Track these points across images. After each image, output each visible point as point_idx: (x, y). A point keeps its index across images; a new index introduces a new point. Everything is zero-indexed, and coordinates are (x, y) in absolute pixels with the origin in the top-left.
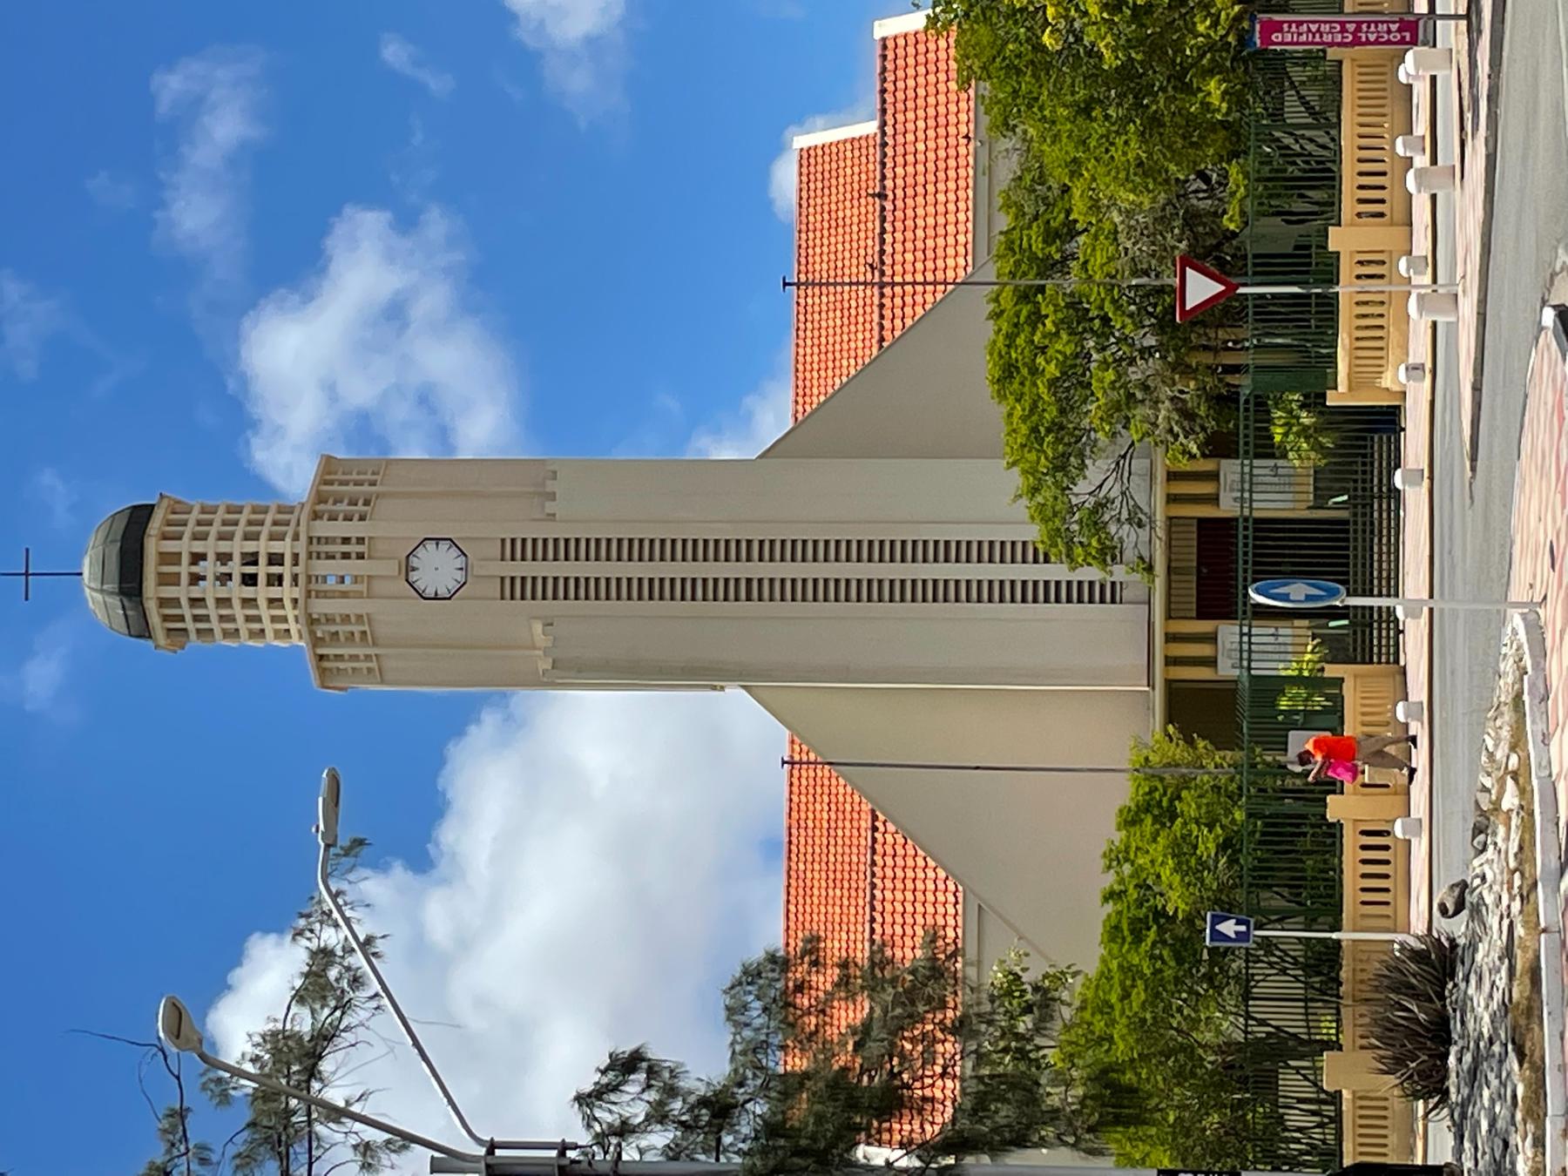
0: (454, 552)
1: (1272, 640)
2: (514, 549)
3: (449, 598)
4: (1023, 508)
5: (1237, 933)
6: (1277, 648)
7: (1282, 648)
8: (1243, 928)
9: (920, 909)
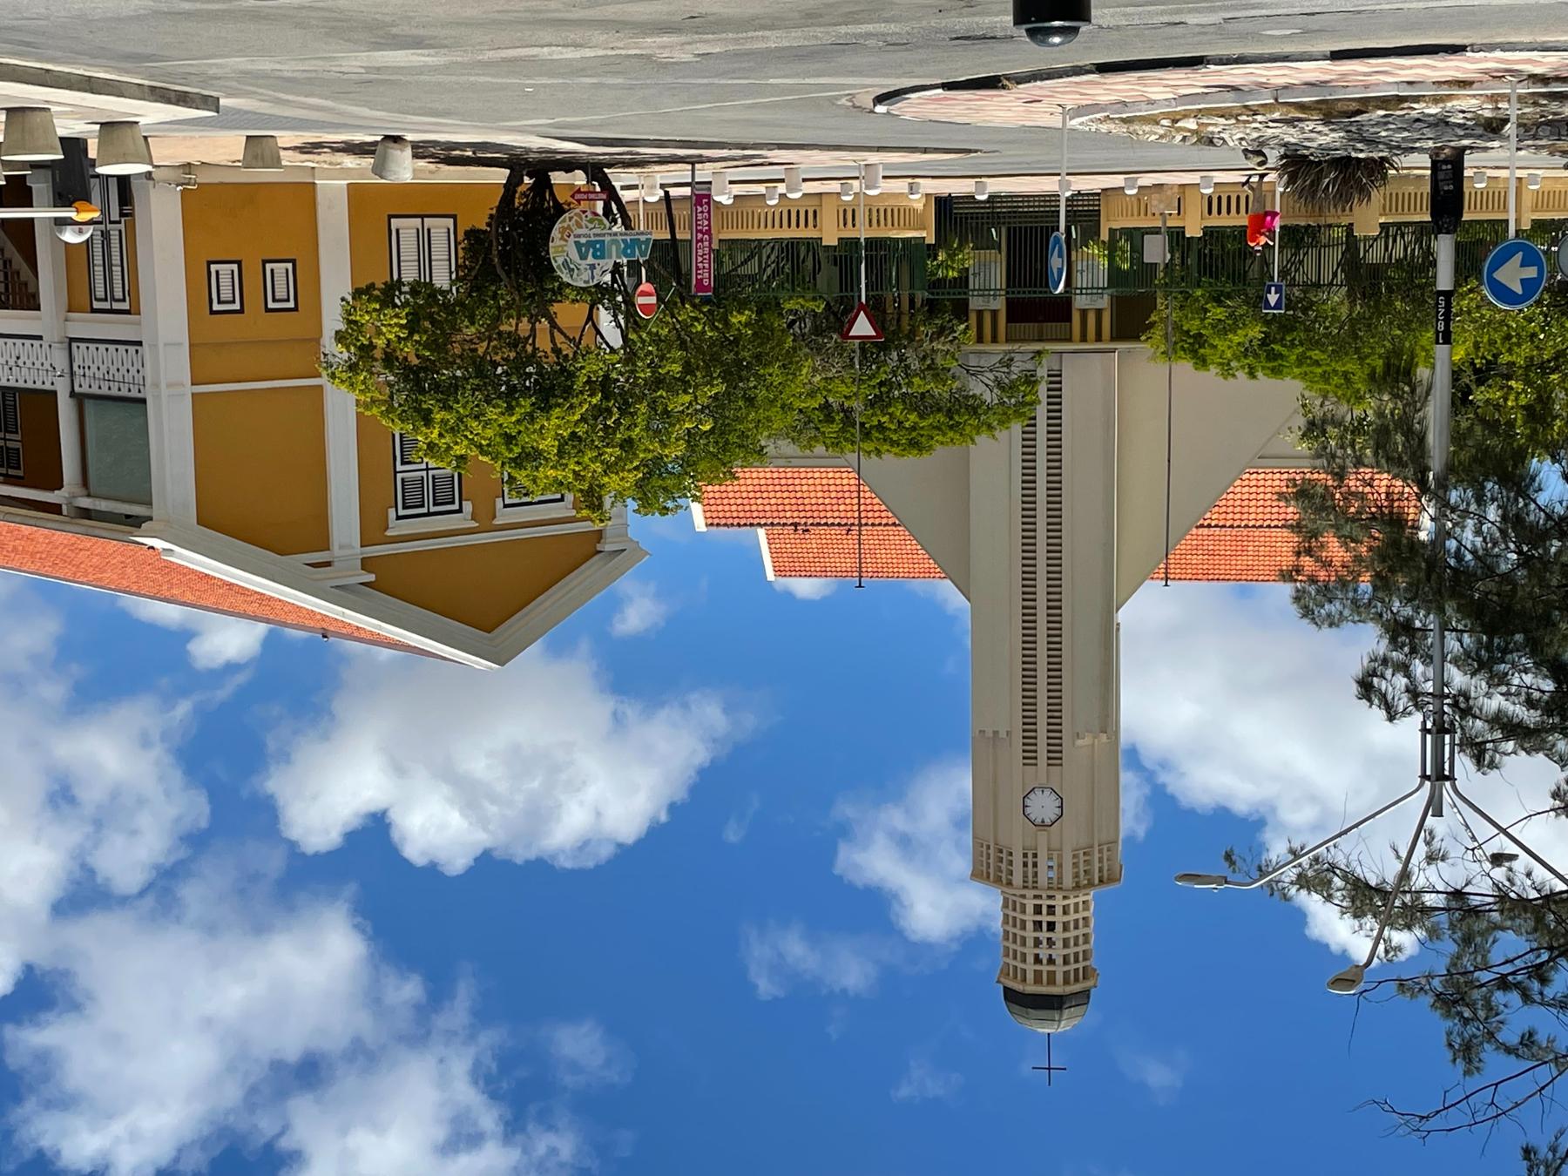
0: (1032, 796)
1: (1085, 274)
4: (1001, 434)
9: (1261, 496)
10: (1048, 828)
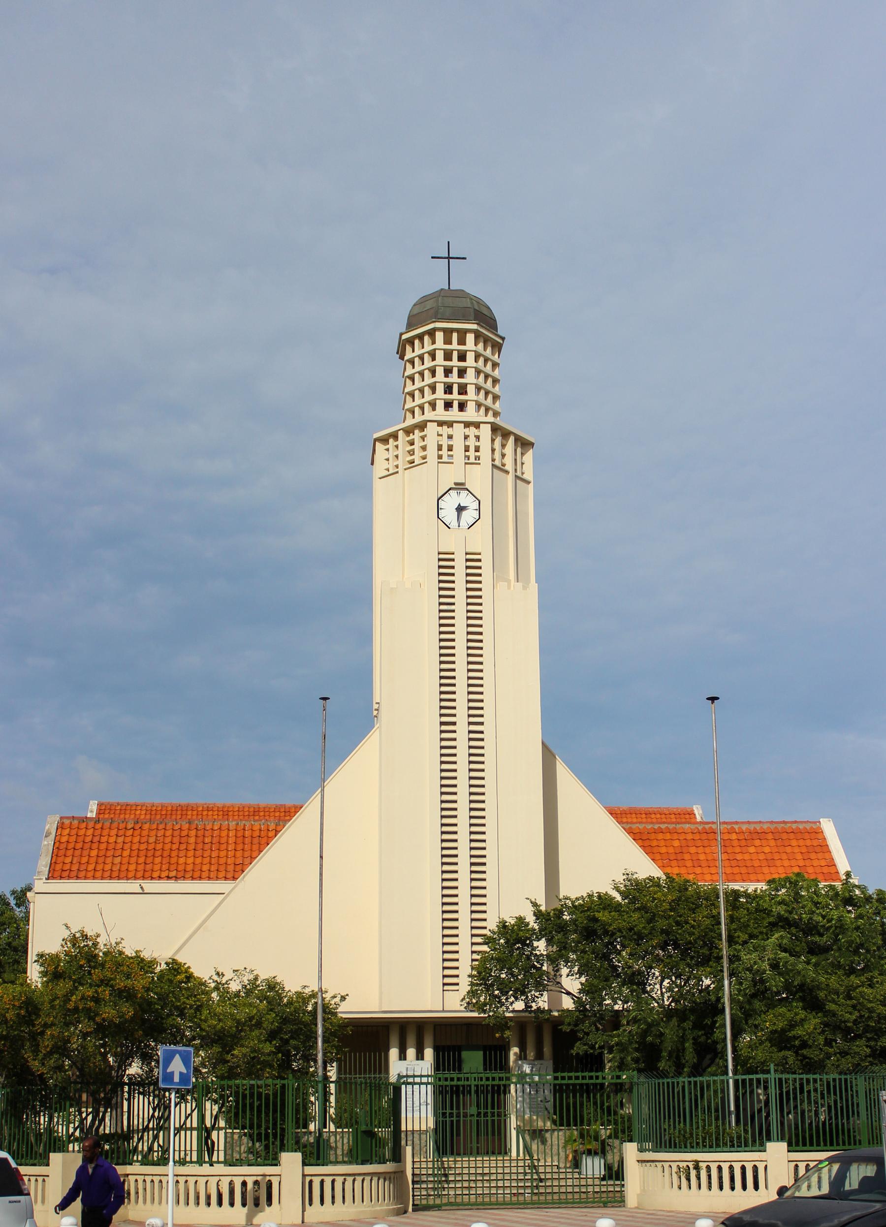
2: (473, 561)
3: (438, 517)
5: (173, 1073)
6: (417, 1103)
7: (417, 1108)
8: (177, 1079)
10: (454, 486)
